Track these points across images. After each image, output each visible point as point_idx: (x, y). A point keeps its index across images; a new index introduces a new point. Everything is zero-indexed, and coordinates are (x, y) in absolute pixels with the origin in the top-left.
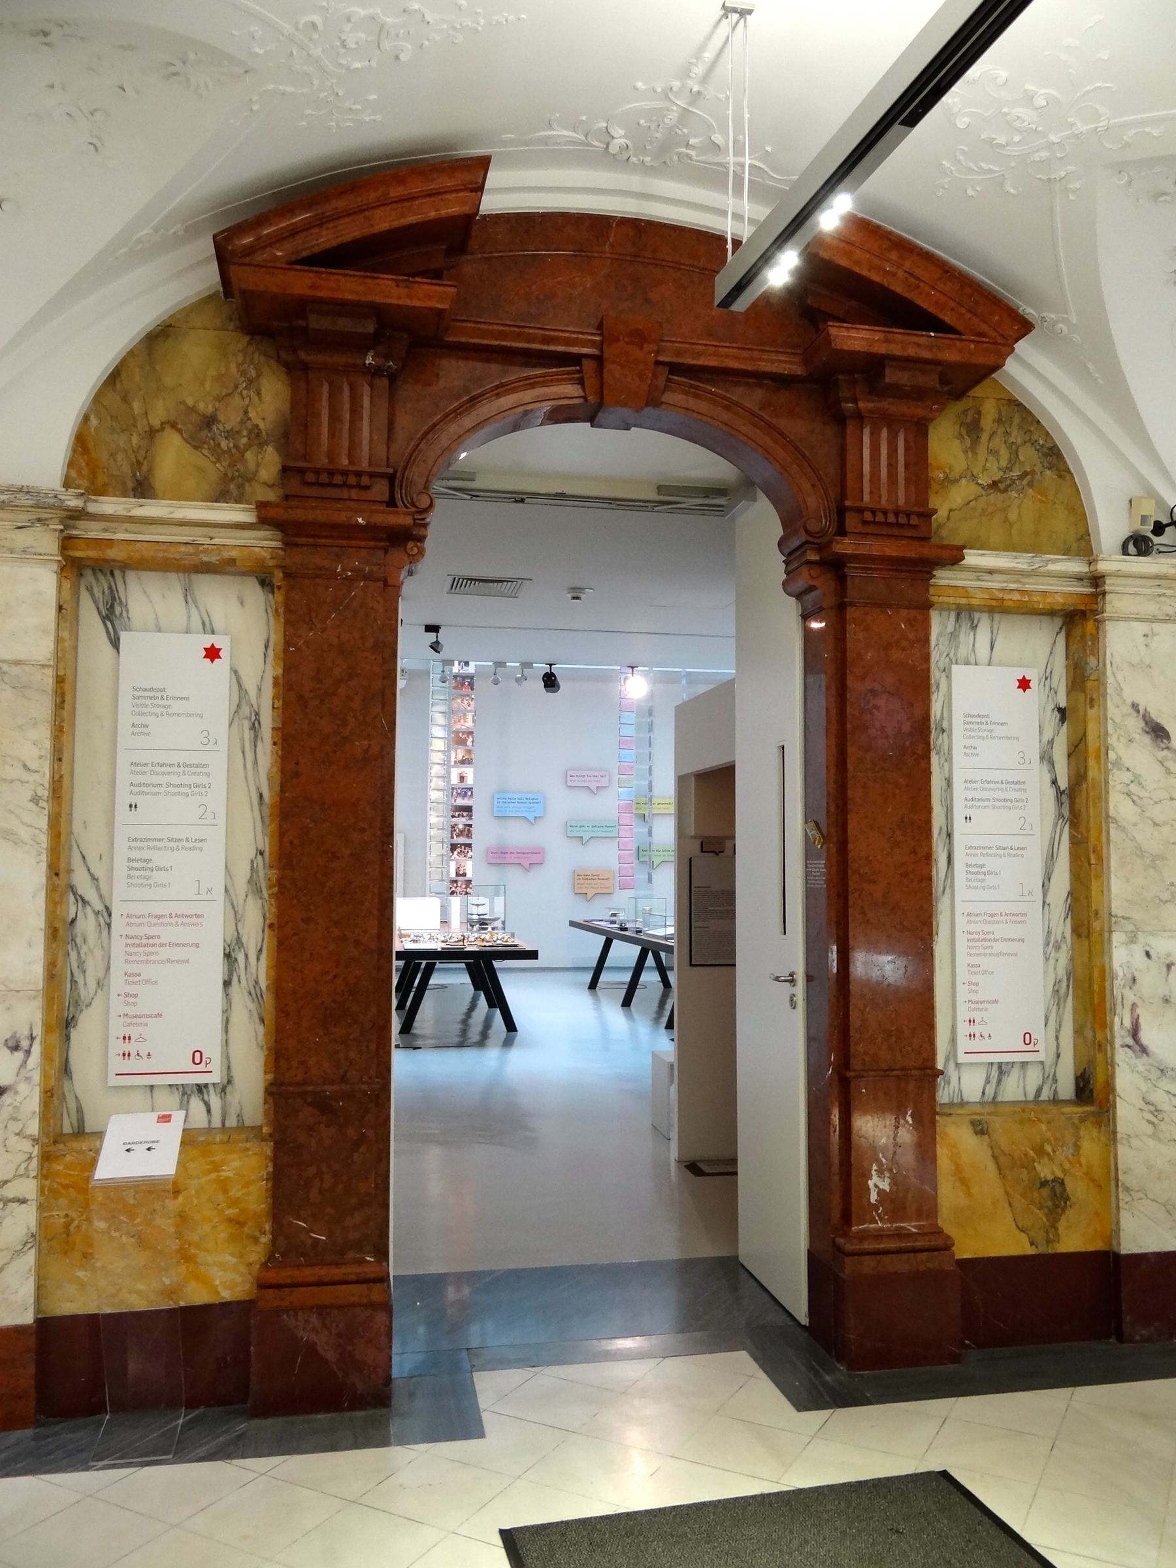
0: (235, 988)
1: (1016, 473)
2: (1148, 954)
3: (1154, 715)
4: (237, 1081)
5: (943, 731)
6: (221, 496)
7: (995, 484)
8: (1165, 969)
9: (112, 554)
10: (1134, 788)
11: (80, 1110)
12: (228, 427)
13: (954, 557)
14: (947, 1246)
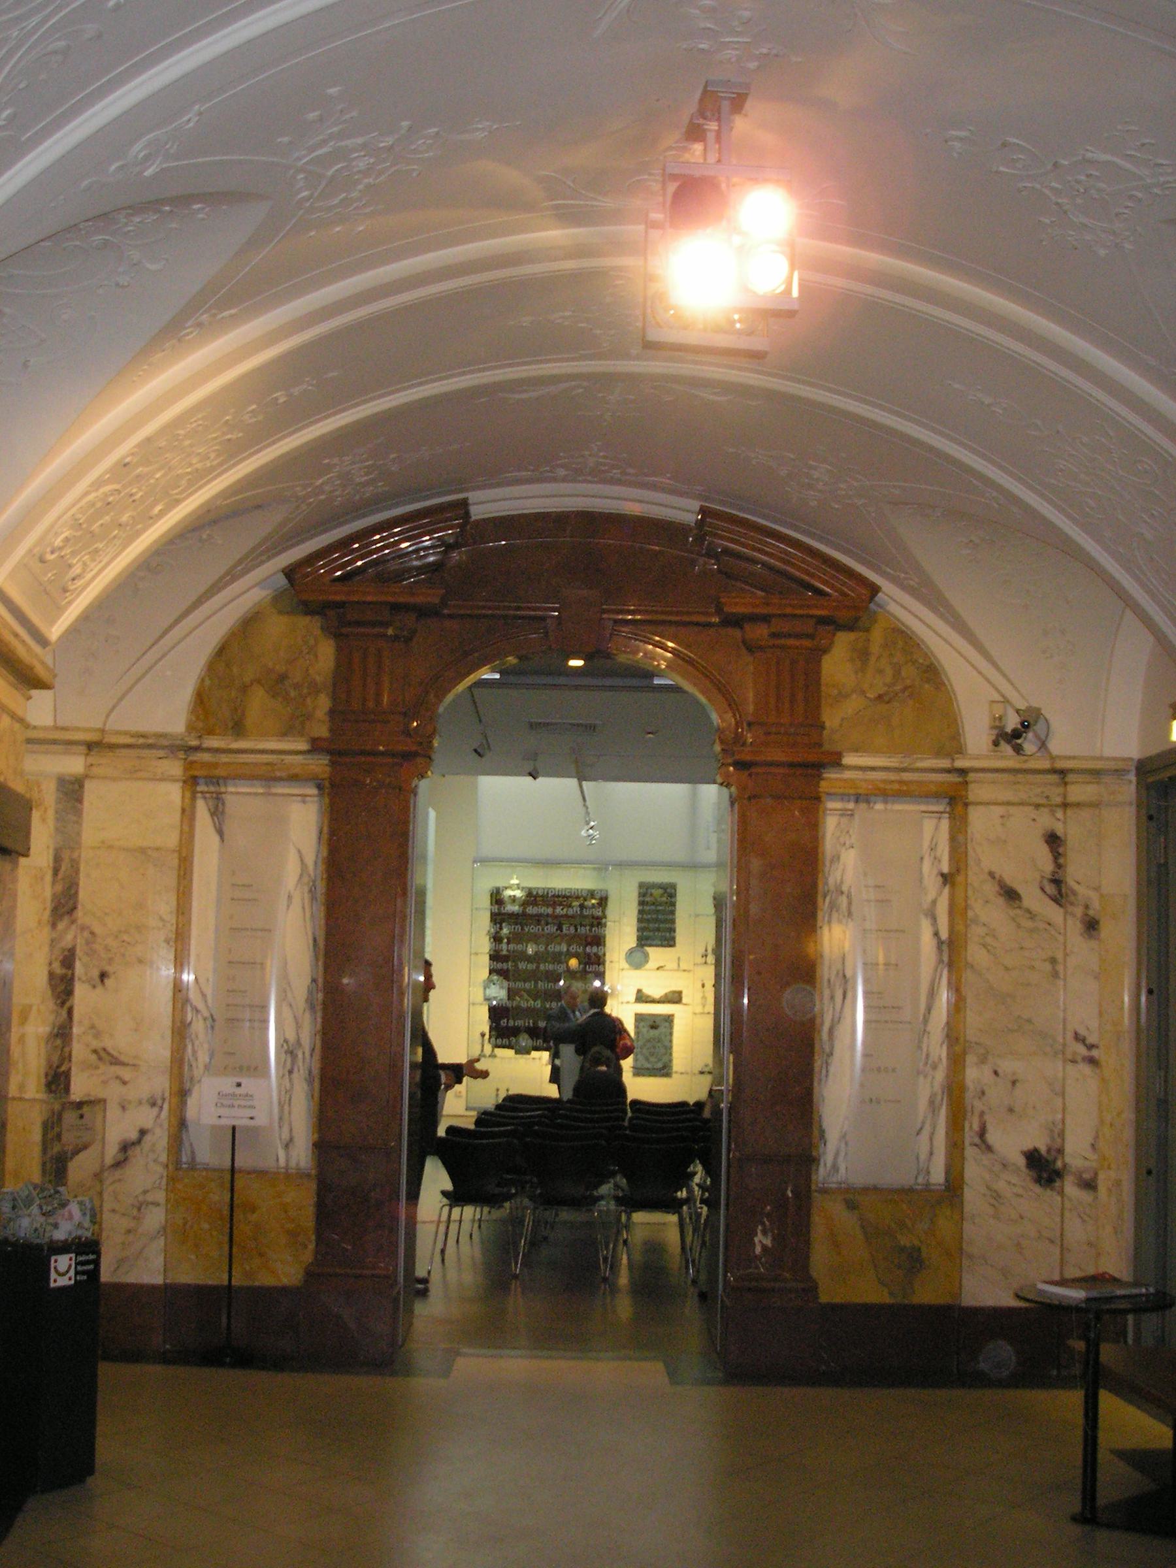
0: (295, 1075)
1: (898, 688)
2: (996, 1073)
3: (1009, 882)
4: (295, 1140)
5: (842, 893)
6: (285, 733)
7: (880, 697)
8: (1009, 1085)
9: (217, 772)
10: (989, 940)
11: (193, 1152)
12: (295, 681)
13: (836, 761)
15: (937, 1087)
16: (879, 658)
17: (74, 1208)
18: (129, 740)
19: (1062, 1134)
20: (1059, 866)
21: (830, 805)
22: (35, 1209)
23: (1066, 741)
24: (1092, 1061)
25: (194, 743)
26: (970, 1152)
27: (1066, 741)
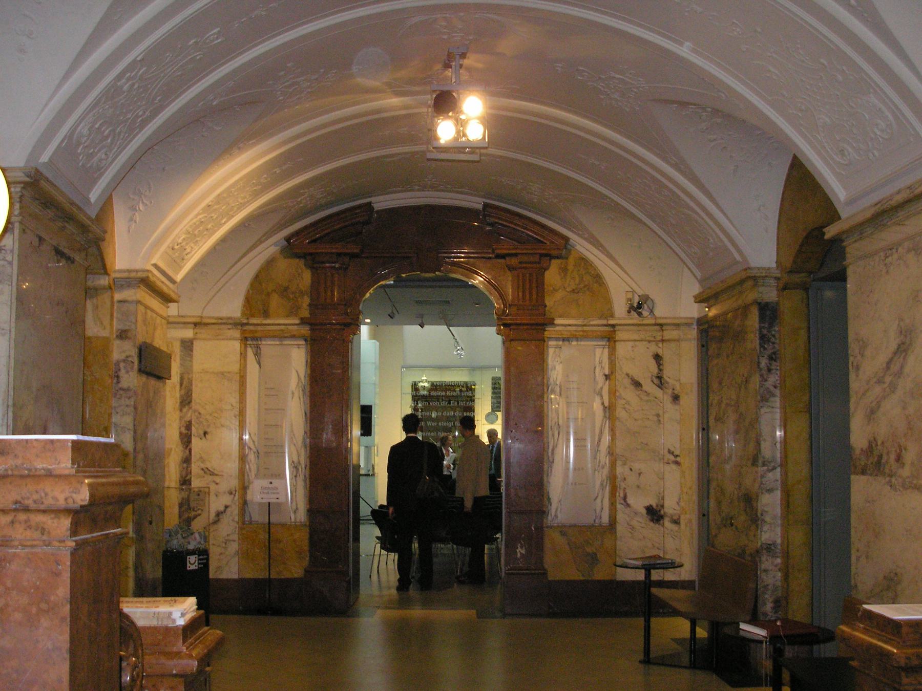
1: (582, 286)
9: (256, 335)
10: (626, 406)
13: (551, 322)
14: (545, 574)
15: (604, 477)
16: (572, 272)
17: (197, 536)
18: (214, 321)
19: (663, 499)
20: (660, 370)
21: (551, 343)
22: (179, 536)
23: (661, 311)
24: (677, 463)
25: (245, 321)
26: (619, 506)
27: (661, 311)
